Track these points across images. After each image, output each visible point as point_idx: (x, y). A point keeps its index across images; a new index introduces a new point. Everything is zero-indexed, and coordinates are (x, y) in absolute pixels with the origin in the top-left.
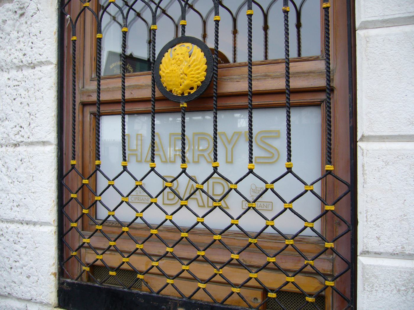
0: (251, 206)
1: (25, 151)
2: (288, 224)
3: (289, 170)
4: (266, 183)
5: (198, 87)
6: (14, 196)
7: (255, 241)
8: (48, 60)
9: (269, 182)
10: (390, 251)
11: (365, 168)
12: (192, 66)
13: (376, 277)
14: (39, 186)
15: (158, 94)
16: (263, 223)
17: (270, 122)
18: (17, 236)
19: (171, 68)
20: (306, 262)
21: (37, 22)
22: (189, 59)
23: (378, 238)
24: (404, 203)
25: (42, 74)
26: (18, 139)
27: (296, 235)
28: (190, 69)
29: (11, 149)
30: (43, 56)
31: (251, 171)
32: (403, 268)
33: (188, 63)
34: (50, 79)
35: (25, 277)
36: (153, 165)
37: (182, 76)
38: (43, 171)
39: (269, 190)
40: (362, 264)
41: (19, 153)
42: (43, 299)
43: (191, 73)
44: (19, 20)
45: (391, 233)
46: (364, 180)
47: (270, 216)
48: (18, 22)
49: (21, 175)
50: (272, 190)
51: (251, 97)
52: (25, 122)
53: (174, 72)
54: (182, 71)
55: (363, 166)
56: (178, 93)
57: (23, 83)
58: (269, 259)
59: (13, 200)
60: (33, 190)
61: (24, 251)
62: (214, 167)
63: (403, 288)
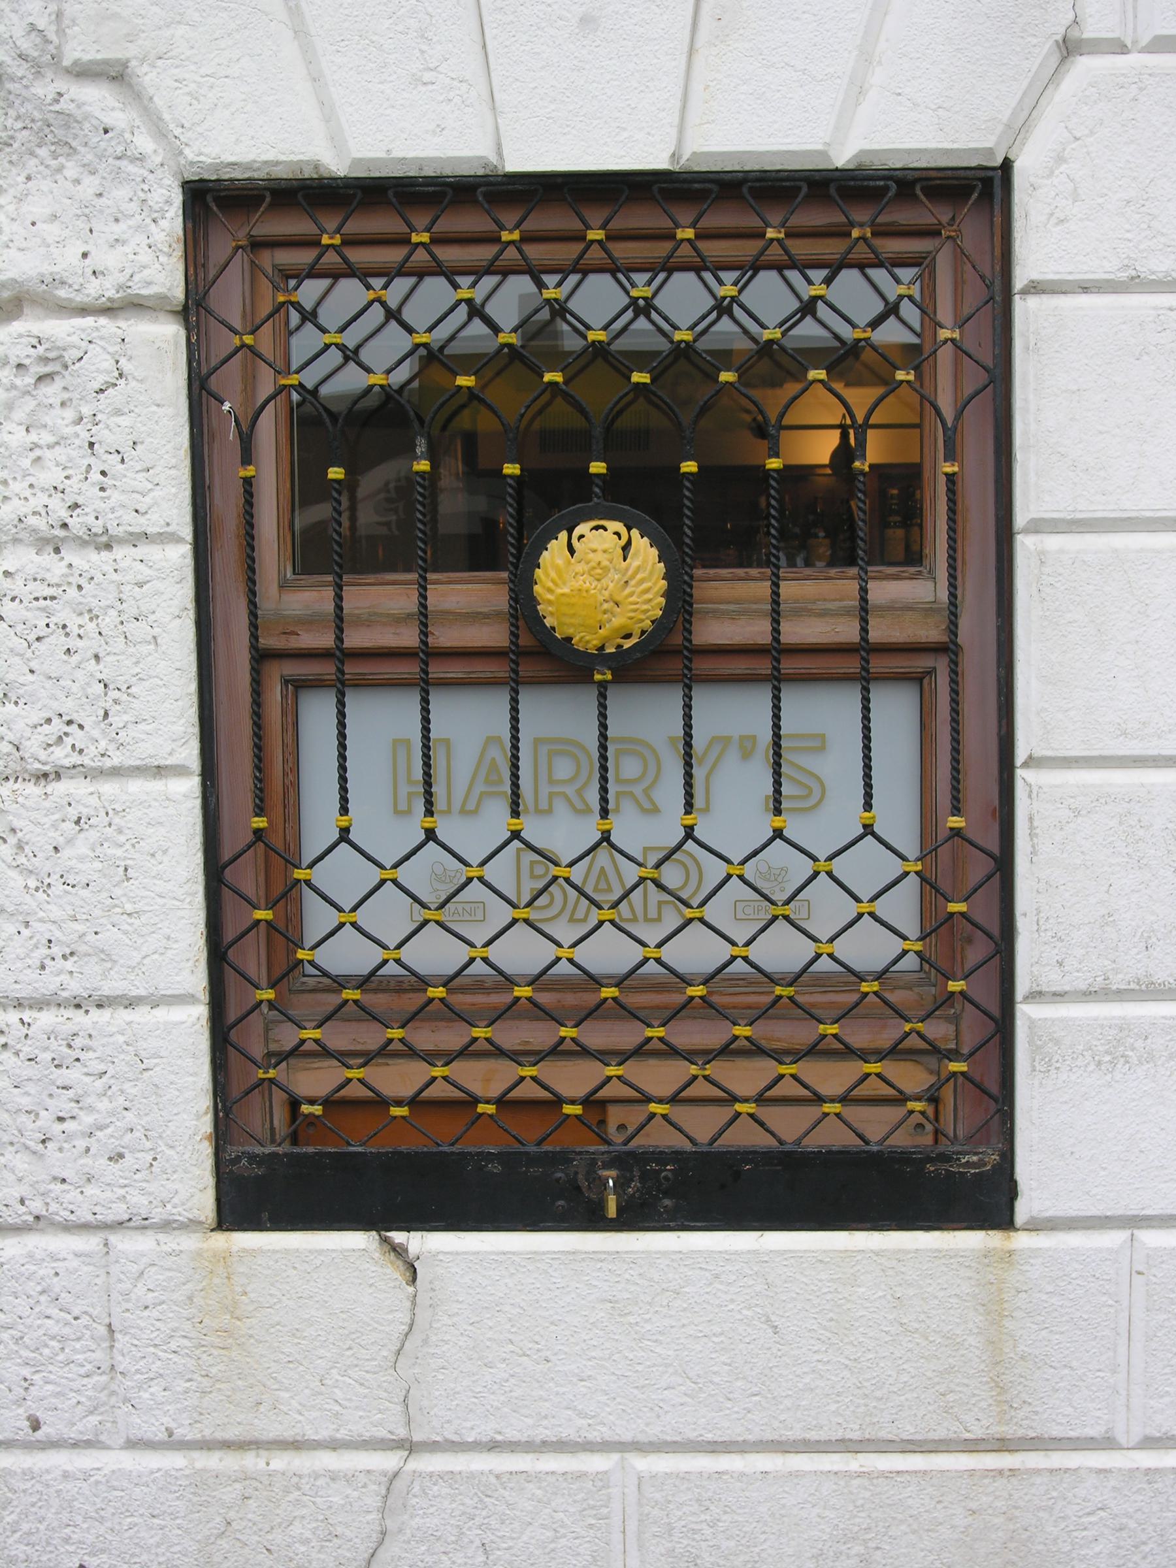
1: (92, 794)
2: (869, 949)
3: (868, 830)
4: (815, 859)
5: (643, 632)
6: (53, 927)
7: (790, 991)
8: (168, 529)
9: (822, 857)
10: (1083, 986)
11: (1035, 824)
12: (633, 583)
13: (1057, 1042)
14: (153, 895)
15: (525, 640)
16: (808, 949)
17: (822, 715)
18: (70, 1046)
19: (576, 584)
20: (907, 1027)
21: (118, 412)
22: (624, 564)
23: (1060, 964)
24: (1107, 892)
25: (148, 572)
26: (61, 756)
27: (886, 970)
28: (628, 591)
29: (32, 790)
30: (148, 516)
31: (778, 834)
32: (1105, 1019)
33: (624, 575)
34: (179, 586)
35: (104, 1161)
36: (515, 823)
37: (606, 606)
38: (165, 852)
39: (823, 875)
40: (1029, 1018)
41: (67, 799)
42: (174, 1211)
43: (631, 599)
44: (34, 393)
45: (1083, 951)
46: (1033, 846)
47: (479, 939)
48: (28, 398)
49: (80, 866)
50: (830, 874)
52: (87, 707)
53: (585, 594)
54: (606, 593)
55: (1031, 819)
56: (590, 646)
57: (72, 592)
58: (825, 1030)
59: (50, 941)
60: (129, 907)
61: (99, 1084)
62: (685, 827)
63: (1107, 1058)
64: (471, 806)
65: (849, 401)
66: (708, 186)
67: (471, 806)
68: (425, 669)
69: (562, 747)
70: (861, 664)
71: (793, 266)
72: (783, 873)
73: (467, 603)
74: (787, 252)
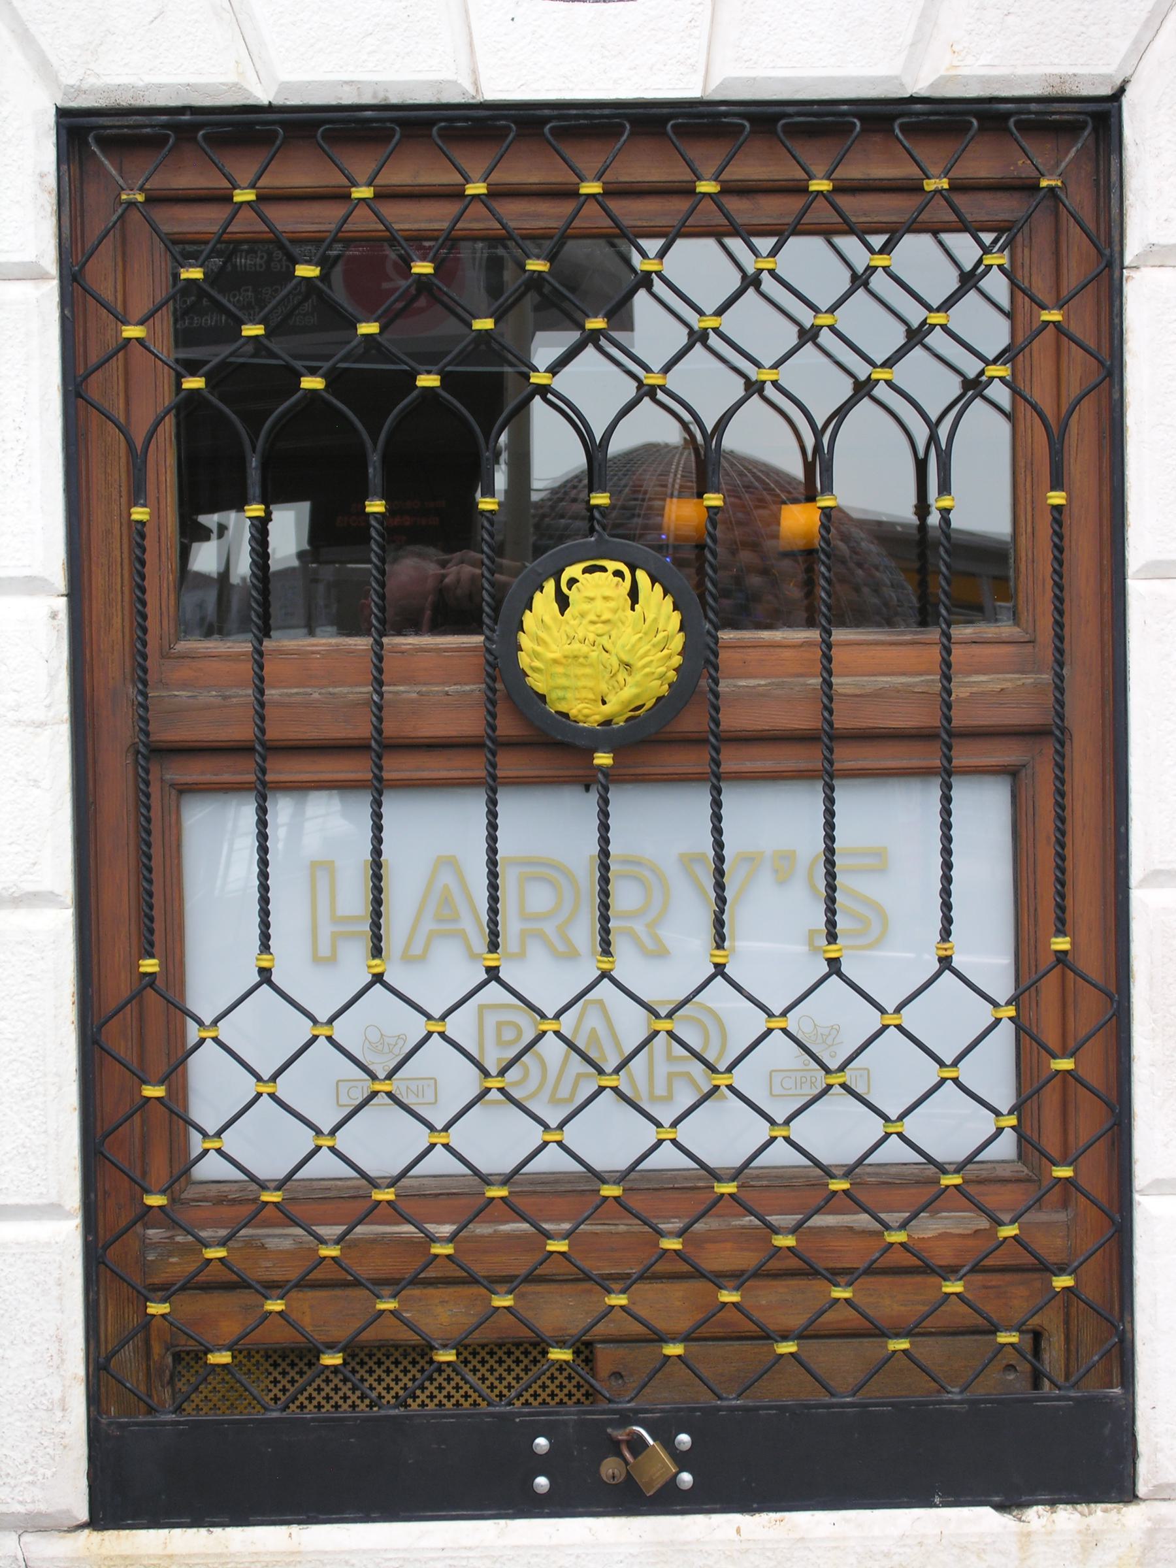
0: (495, 1085)
2: (955, 1130)
15: (507, 727)
17: (888, 821)
51: (494, 754)
64: (417, 950)
65: (151, 419)
66: (1081, 118)
67: (417, 950)
68: (375, 761)
69: (543, 869)
70: (937, 749)
71: (735, 233)
72: (834, 1032)
73: (434, 670)
74: (726, 215)
